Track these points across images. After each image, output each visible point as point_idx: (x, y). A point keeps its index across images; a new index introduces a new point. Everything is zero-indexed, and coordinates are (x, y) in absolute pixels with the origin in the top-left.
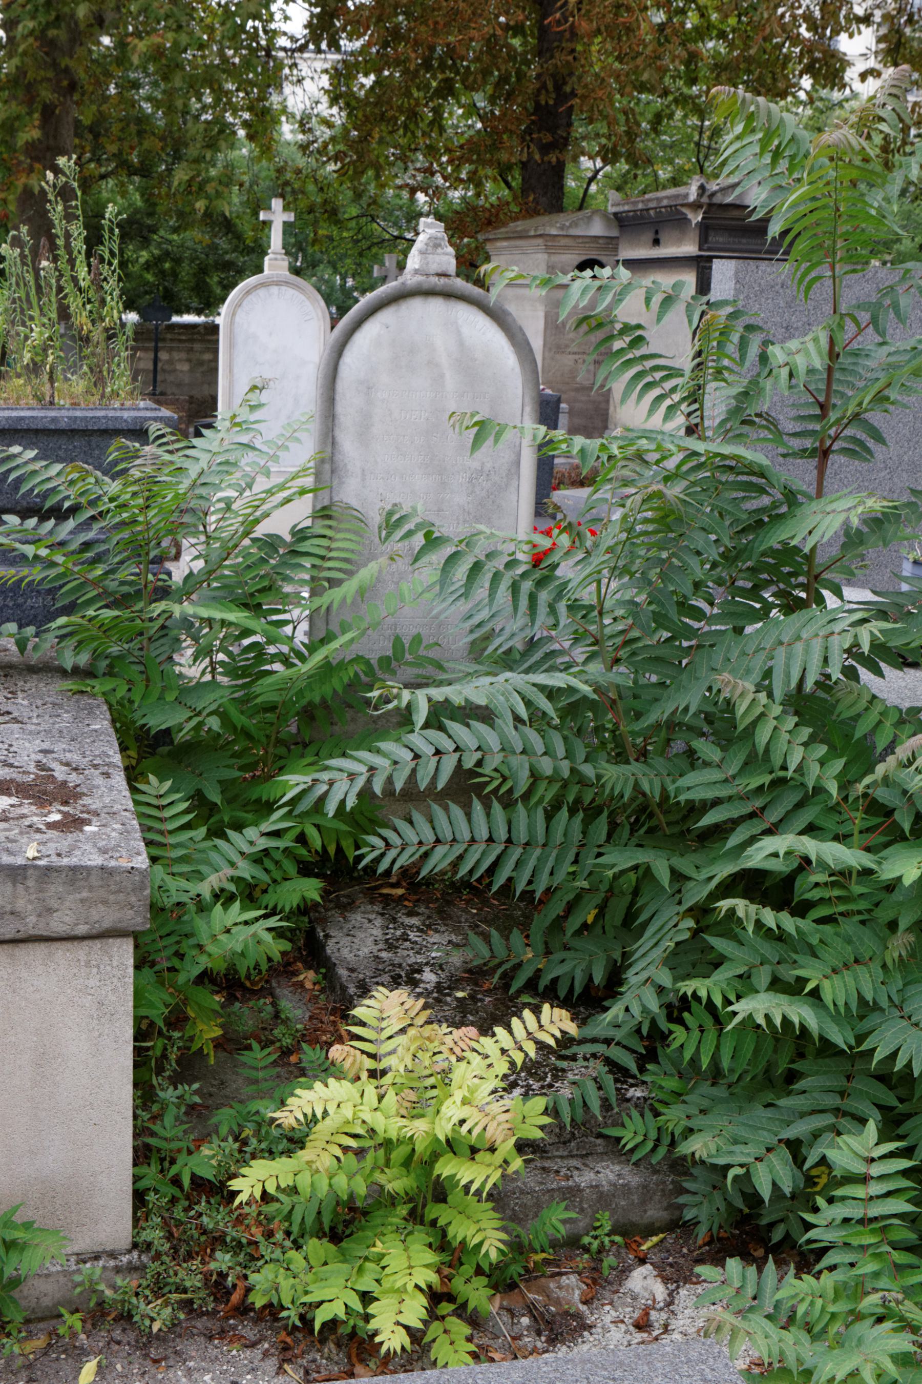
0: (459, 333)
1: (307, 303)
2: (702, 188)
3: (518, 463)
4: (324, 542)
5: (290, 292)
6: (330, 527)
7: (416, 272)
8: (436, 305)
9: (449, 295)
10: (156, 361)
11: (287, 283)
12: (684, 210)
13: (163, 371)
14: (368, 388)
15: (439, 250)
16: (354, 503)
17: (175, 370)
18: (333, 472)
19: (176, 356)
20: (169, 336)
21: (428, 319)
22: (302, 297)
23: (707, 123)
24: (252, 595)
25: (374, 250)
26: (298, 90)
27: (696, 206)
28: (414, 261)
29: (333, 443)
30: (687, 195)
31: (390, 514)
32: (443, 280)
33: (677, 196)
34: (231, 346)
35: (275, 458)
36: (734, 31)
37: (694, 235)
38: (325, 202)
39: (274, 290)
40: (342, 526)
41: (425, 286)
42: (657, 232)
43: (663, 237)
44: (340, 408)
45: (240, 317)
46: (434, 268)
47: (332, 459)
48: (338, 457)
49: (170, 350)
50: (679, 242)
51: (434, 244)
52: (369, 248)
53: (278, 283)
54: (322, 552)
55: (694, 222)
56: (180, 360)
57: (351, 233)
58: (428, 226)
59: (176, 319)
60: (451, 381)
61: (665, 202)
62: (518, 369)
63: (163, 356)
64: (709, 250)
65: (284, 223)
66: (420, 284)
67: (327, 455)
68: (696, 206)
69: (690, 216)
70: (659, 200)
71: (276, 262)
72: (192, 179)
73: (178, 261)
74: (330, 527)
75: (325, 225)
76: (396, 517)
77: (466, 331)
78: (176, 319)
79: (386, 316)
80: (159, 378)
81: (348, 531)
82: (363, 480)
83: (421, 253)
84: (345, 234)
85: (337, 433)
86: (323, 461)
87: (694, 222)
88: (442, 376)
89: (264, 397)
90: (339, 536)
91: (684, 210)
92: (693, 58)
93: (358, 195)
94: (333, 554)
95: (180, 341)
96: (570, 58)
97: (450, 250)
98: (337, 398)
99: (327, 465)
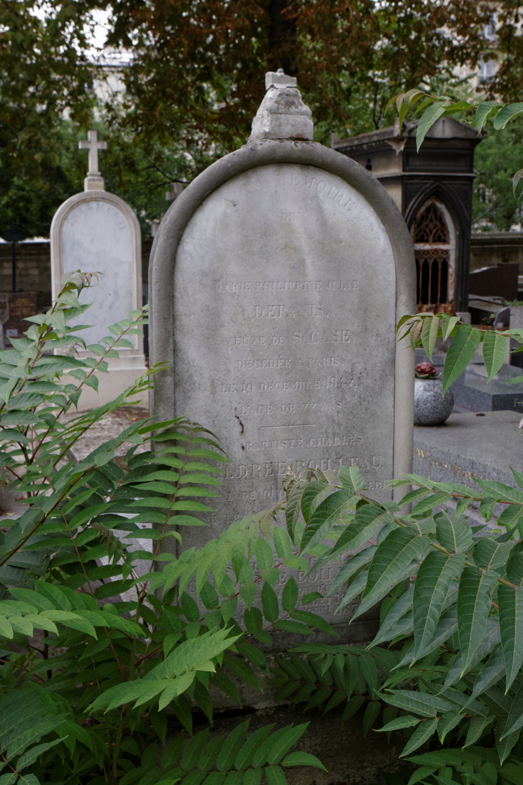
0: (320, 210)
1: (121, 214)
2: (404, 126)
3: (393, 362)
4: (171, 477)
5: (106, 206)
6: (176, 456)
7: (267, 136)
8: (292, 178)
9: (308, 163)
10: (14, 268)
11: (104, 199)
12: (390, 143)
13: (21, 275)
14: (214, 280)
15: (293, 109)
16: (203, 421)
17: (29, 275)
18: (176, 385)
19: (29, 264)
20: (24, 251)
21: (283, 193)
22: (117, 210)
23: (379, 97)
24: (83, 549)
25: (159, 189)
26: (104, 84)
27: (398, 140)
28: (261, 123)
29: (175, 351)
30: (392, 132)
31: (310, 494)
32: (300, 145)
33: (384, 133)
34: (61, 251)
35: (102, 366)
36: (395, 32)
37: (399, 161)
38: (126, 158)
39: (94, 205)
40: (192, 454)
41: (280, 153)
42: (369, 161)
43: (373, 164)
44: (181, 307)
45: (67, 227)
46: (287, 130)
47: (174, 371)
48: (181, 367)
49: (25, 261)
50: (387, 166)
51: (286, 102)
52: (156, 188)
53: (96, 199)
54: (170, 490)
55: (398, 151)
56: (32, 268)
57: (143, 179)
58: (278, 80)
59: (28, 241)
60: (312, 268)
61: (375, 138)
62: (389, 251)
63: (20, 265)
64: (410, 171)
65: (98, 150)
66: (273, 150)
67: (168, 366)
68: (398, 140)
69: (394, 147)
70: (370, 137)
71: (93, 183)
72: (31, 138)
73: (28, 200)
74: (176, 456)
75: (127, 173)
76: (319, 499)
77: (328, 206)
78: (28, 241)
79: (232, 191)
80: (18, 280)
81: (198, 460)
82: (214, 392)
83: (272, 112)
84: (140, 179)
85: (179, 337)
86: (163, 374)
87: (398, 151)
88: (302, 262)
89: (86, 296)
90: (189, 467)
91: (390, 143)
92: (368, 52)
93: (148, 151)
94: (183, 492)
95: (31, 254)
96: (293, 46)
97: (306, 108)
98: (178, 294)
99: (168, 377)
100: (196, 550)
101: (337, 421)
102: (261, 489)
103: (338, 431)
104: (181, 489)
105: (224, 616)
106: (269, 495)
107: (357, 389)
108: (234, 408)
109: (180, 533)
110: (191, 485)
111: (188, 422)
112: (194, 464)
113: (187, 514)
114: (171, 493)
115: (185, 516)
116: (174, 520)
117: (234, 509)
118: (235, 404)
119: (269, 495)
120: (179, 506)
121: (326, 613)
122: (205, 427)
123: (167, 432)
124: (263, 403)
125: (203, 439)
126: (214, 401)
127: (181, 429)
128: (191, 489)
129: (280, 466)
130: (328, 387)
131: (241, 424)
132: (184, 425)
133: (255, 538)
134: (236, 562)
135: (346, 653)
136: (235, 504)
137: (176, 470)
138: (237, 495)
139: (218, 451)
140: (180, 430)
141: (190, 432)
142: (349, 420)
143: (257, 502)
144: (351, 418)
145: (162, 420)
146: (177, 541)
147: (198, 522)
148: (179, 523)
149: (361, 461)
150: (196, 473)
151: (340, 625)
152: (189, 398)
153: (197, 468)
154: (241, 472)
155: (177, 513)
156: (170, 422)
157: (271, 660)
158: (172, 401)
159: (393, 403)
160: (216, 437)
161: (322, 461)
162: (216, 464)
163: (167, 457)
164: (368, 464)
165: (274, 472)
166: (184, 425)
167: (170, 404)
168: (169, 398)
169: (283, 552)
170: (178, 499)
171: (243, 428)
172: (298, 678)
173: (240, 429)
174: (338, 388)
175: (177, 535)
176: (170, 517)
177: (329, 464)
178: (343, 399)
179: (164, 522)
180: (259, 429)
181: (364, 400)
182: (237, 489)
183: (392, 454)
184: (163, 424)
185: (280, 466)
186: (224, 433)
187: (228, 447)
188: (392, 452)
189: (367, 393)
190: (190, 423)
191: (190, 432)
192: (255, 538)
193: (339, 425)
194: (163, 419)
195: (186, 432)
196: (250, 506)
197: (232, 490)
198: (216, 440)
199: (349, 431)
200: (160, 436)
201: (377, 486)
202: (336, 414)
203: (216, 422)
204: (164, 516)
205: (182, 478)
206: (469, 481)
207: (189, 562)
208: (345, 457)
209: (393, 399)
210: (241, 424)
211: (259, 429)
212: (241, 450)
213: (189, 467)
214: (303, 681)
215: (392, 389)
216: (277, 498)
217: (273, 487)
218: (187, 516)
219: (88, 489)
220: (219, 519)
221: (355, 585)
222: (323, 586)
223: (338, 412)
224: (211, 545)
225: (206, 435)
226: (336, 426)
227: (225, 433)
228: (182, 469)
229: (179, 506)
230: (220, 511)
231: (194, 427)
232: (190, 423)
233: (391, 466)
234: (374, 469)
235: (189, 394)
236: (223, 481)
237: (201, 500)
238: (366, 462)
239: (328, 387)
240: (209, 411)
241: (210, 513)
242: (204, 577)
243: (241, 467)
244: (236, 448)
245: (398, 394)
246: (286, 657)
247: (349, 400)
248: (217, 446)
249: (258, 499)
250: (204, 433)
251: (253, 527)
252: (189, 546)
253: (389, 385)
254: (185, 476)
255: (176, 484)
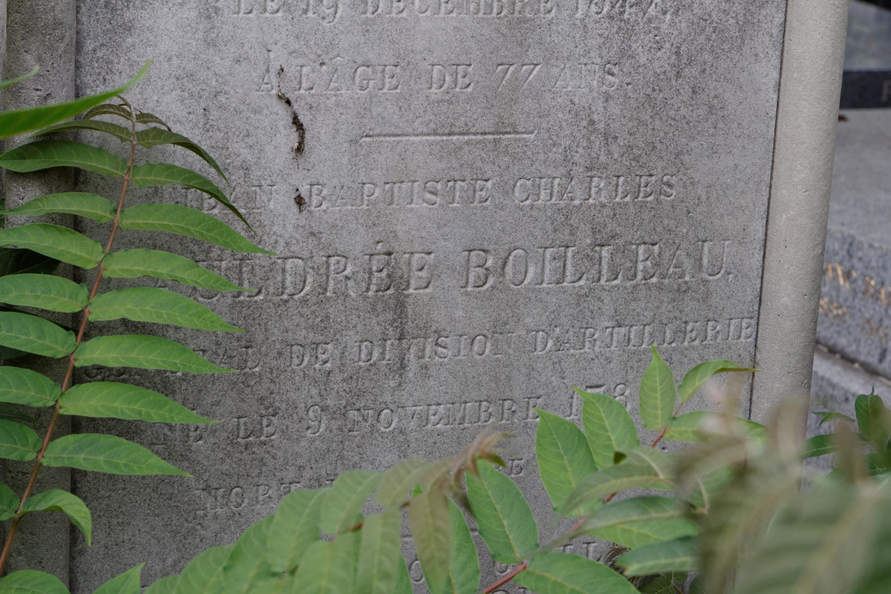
4: (60, 296)
6: (76, 224)
16: (172, 109)
40: (134, 219)
54: (52, 343)
74: (76, 224)
81: (151, 242)
90: (122, 265)
101: (601, 126)
102: (351, 338)
103: (603, 158)
104: (92, 342)
106: (376, 355)
107: (672, 24)
108: (274, 70)
110: (129, 327)
111: (121, 110)
112: (137, 254)
114: (59, 352)
116: (64, 452)
117: (261, 400)
118: (278, 58)
119: (376, 355)
120: (85, 401)
122: (176, 129)
123: (50, 140)
124: (372, 57)
125: (171, 170)
126: (211, 44)
127: (97, 133)
128: (127, 340)
129: (415, 264)
130: (579, 15)
131: (297, 122)
132: (107, 118)
136: (266, 384)
137: (77, 275)
138: (273, 354)
139: (218, 211)
140: (92, 137)
141: (127, 146)
142: (641, 122)
144: (646, 116)
145: (31, 101)
146: (74, 530)
149: (667, 255)
150: (142, 287)
152: (128, 28)
153: (150, 271)
154: (289, 279)
155: (76, 425)
156: (64, 110)
158: (70, 34)
159: (775, 75)
160: (216, 167)
161: (549, 252)
162: (208, 251)
163: (45, 227)
164: (688, 265)
165: (395, 282)
166: (107, 118)
167: (62, 46)
168: (58, 24)
170: (81, 376)
171: (302, 137)
173: (293, 139)
174: (612, 18)
175: (76, 508)
176: (52, 439)
177: (569, 266)
178: (626, 53)
179: (30, 456)
180: (354, 142)
181: (690, 63)
182: (276, 334)
183: (760, 235)
184: (35, 117)
185: (415, 264)
186: (241, 151)
187: (251, 198)
188: (762, 230)
189: (702, 39)
190: (128, 115)
191: (127, 146)
193: (608, 137)
194: (35, 95)
195: (114, 141)
196: (314, 392)
197: (260, 338)
198: (220, 184)
199: (636, 159)
200: (24, 152)
201: (710, 333)
202: (600, 104)
203: (214, 114)
204: (32, 436)
205: (96, 300)
206: (838, 289)
208: (620, 242)
209: (777, 62)
210: (297, 122)
211: (354, 142)
212: (295, 208)
213: (122, 265)
215: (775, 32)
216: (403, 367)
217: (391, 332)
218: (114, 439)
220: (214, 432)
223: (608, 98)
225: (182, 157)
226: (598, 140)
227: (244, 152)
228: (98, 269)
229: (85, 401)
230: (218, 403)
231: (140, 127)
232: (128, 115)
233: (756, 273)
234: (705, 282)
235: (128, 15)
236: (232, 307)
237: (160, 383)
238: (683, 258)
239: (579, 15)
240: (191, 76)
243: (289, 264)
244: (277, 204)
245: (794, 47)
247: (643, 59)
248: (216, 194)
249: (342, 367)
250: (171, 147)
253: (771, 17)
254: (108, 296)
255: (73, 323)
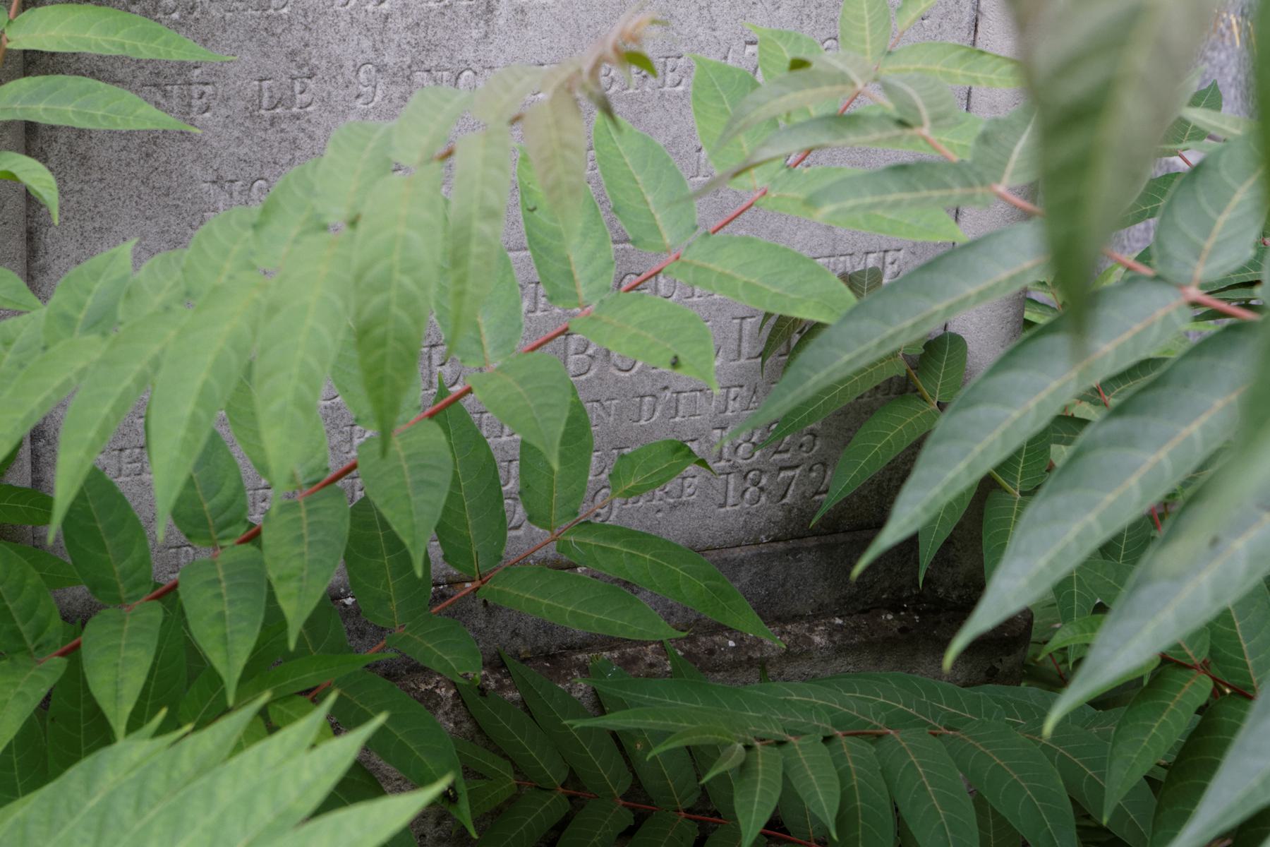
100: (137, 261)
105: (280, 592)
109: (42, 157)
113: (77, 72)
115: (71, 82)
117: (293, 54)
121: (673, 507)
133: (491, 214)
134: (382, 343)
135: (826, 726)
136: (298, 31)
143: (398, 23)
146: (31, 200)
147: (138, 113)
148: (41, 113)
151: (728, 554)
157: (439, 702)
169: (569, 275)
172: (553, 772)
192: (491, 214)
196: (366, 44)
207: (102, 322)
214: (577, 789)
219: (1082, 398)
221: (1060, 501)
222: (668, 393)
224: (223, 237)
241: (183, 67)
242: (194, 422)
246: (501, 687)
251: (471, 153)
252: (95, 235)
